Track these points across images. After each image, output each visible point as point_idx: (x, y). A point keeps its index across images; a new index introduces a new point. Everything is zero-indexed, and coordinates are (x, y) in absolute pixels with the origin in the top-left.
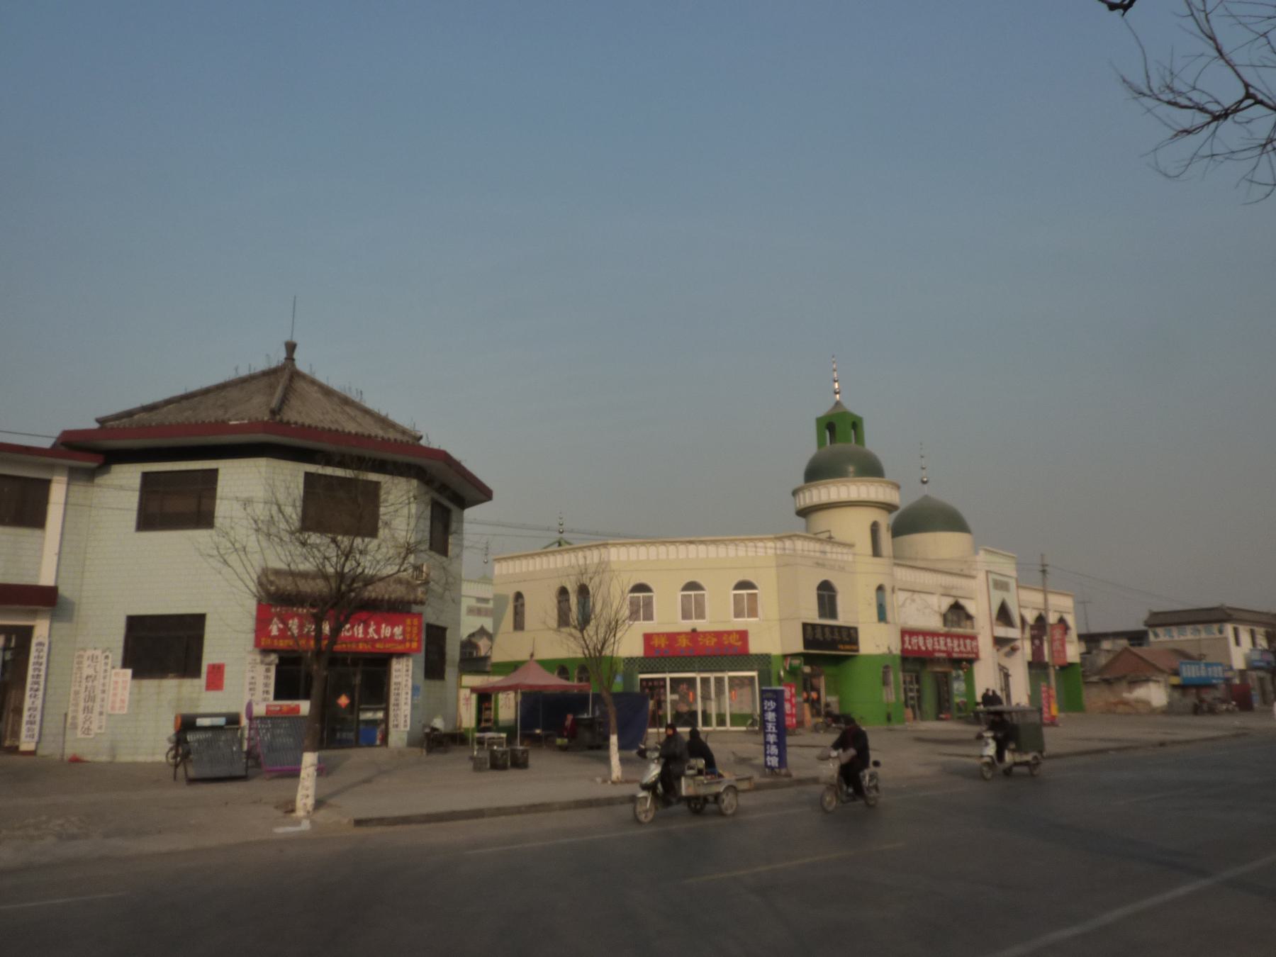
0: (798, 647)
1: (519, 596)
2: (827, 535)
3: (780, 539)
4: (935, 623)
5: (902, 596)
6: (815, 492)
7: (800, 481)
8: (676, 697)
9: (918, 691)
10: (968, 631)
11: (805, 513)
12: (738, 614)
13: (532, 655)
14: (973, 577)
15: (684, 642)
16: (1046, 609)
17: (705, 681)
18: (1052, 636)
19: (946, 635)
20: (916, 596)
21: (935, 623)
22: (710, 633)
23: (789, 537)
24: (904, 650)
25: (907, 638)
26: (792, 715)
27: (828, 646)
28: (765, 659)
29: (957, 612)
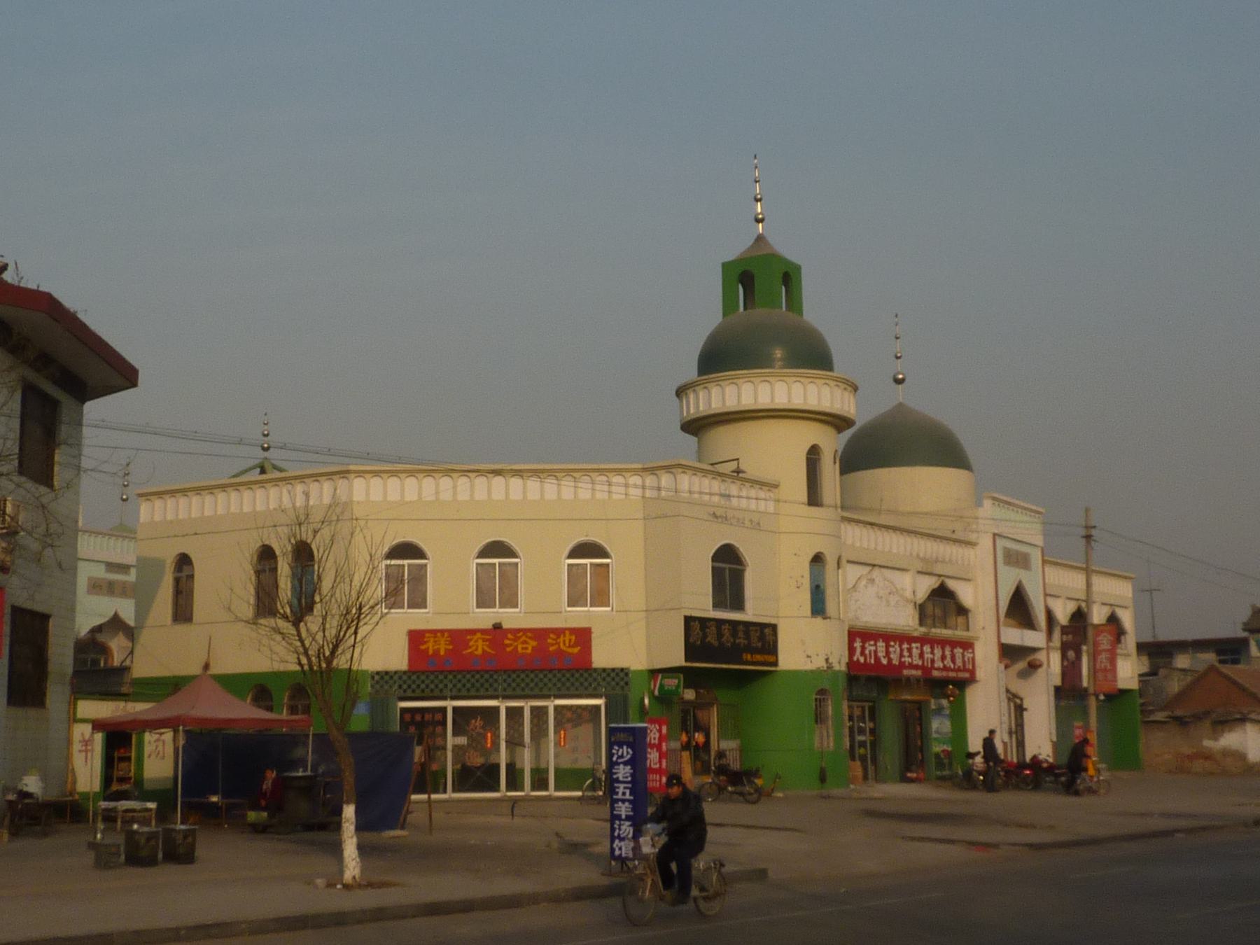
0: (677, 657)
1: (184, 561)
2: (733, 466)
3: (652, 470)
4: (904, 619)
5: (852, 572)
8: (462, 740)
9: (873, 732)
10: (960, 634)
11: (696, 427)
13: (207, 667)
15: (479, 647)
16: (1089, 601)
17: (514, 714)
18: (1096, 644)
19: (923, 640)
21: (904, 619)
22: (525, 631)
23: (668, 468)
24: (851, 664)
25: (858, 644)
27: (726, 654)
28: (620, 676)
29: (942, 603)
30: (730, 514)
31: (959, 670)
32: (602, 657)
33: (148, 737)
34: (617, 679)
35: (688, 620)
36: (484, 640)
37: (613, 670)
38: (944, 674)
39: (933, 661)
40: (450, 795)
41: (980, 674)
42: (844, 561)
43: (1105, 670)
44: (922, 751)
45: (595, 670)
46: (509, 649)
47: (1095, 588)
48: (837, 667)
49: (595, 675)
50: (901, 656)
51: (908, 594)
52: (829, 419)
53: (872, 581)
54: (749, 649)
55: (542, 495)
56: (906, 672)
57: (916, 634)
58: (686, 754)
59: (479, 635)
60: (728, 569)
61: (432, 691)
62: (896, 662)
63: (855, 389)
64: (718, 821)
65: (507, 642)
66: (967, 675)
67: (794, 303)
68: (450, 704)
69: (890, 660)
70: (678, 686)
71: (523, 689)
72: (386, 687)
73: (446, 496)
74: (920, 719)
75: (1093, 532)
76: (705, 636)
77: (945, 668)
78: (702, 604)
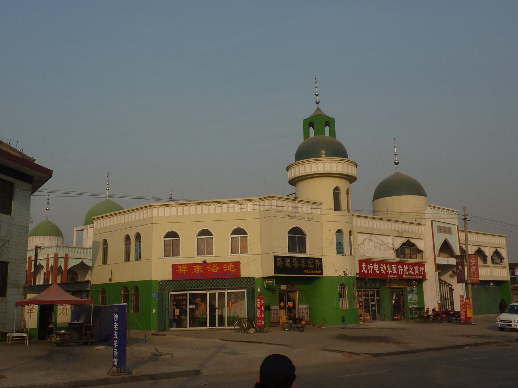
0: (271, 272)
1: (105, 241)
2: (294, 196)
3: (262, 199)
4: (390, 255)
5: (361, 238)
6: (302, 167)
7: (293, 160)
8: (193, 307)
9: (378, 300)
10: (418, 260)
11: (294, 182)
12: (234, 251)
13: (110, 280)
14: (423, 225)
15: (198, 270)
16: (466, 244)
17: (212, 296)
18: (470, 263)
19: (398, 264)
20: (373, 237)
21: (390, 255)
22: (215, 263)
23: (267, 198)
24: (360, 273)
25: (364, 265)
26: (261, 318)
27: (296, 271)
28: (252, 280)
29: (408, 248)
30: (297, 215)
31: (417, 274)
32: (245, 273)
33: (59, 307)
34: (250, 281)
35: (275, 257)
36: (200, 267)
37: (249, 278)
38: (409, 277)
39: (403, 272)
40: (188, 328)
41: (427, 277)
42: (354, 233)
43: (474, 273)
44: (404, 308)
45: (242, 278)
46: (225, 270)
47: (469, 239)
48: (349, 275)
49: (242, 280)
50: (387, 269)
51: (391, 245)
52: (345, 177)
53: (371, 240)
54: (307, 268)
55: (215, 212)
56: (389, 276)
57: (394, 261)
58: (283, 311)
59: (198, 266)
60: (297, 238)
61: (174, 288)
62: (384, 272)
63: (356, 165)
64: (260, 341)
65: (224, 267)
66: (421, 277)
67: (332, 133)
68: (188, 293)
69: (381, 272)
70: (273, 284)
71: (211, 286)
72: (164, 286)
73: (186, 213)
74: (402, 295)
75: (467, 217)
76: (284, 263)
77: (410, 274)
78: (284, 251)
